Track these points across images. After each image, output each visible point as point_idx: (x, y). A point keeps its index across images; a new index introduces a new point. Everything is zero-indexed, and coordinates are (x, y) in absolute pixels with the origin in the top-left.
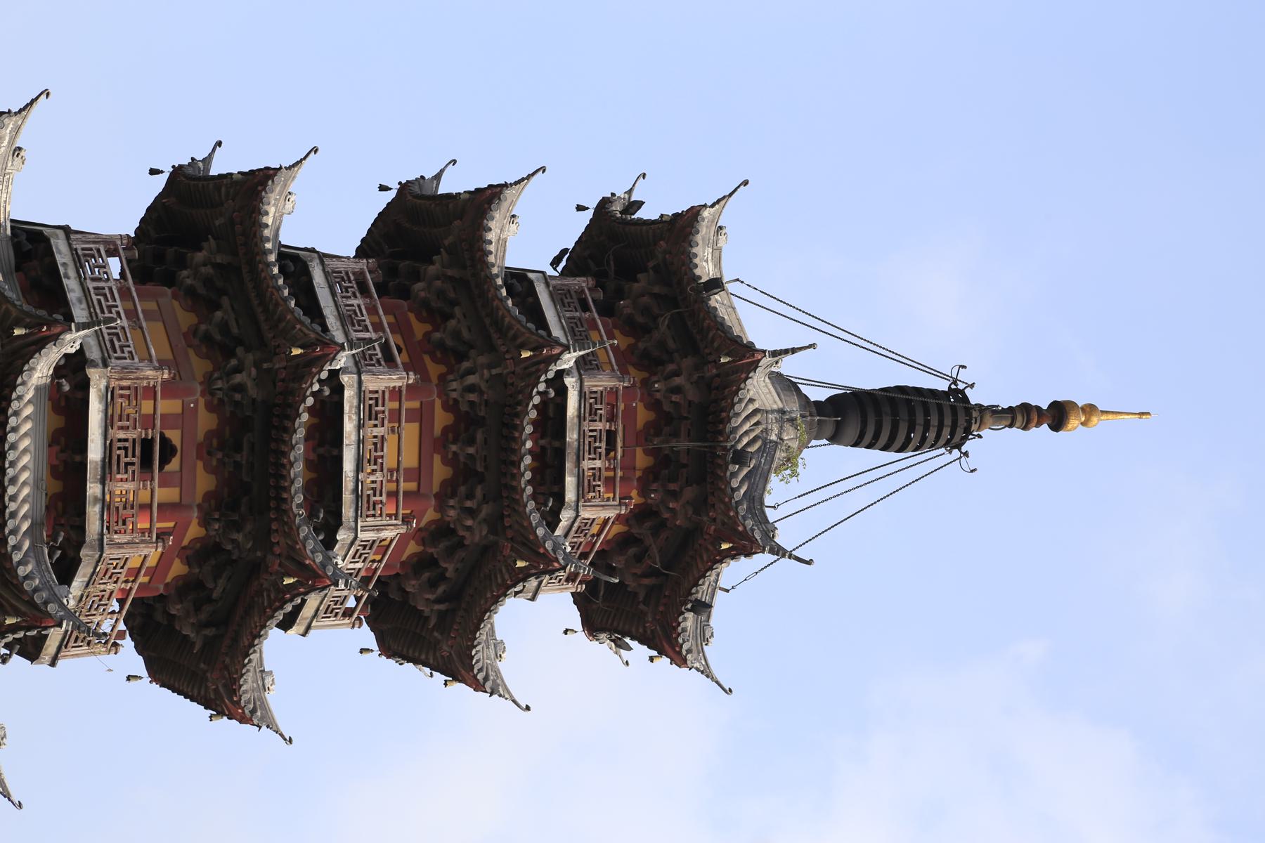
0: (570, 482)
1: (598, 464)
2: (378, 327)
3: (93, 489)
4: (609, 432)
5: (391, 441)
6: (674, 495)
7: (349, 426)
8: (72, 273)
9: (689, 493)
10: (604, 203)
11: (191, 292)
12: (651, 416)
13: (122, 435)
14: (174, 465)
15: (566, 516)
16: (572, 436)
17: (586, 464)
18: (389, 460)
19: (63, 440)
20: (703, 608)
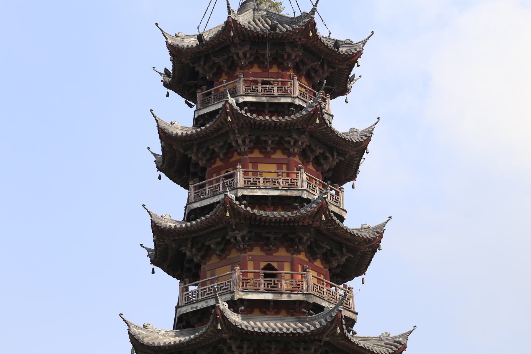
0: (283, 100)
1: (276, 88)
2: (218, 181)
3: (285, 297)
4: (263, 84)
6: (289, 56)
7: (259, 193)
9: (288, 49)
10: (166, 85)
11: (203, 257)
12: (256, 66)
13: (262, 286)
14: (275, 265)
15: (298, 102)
16: (264, 99)
17: (276, 93)
18: (274, 176)
19: (264, 310)
20: (337, 44)
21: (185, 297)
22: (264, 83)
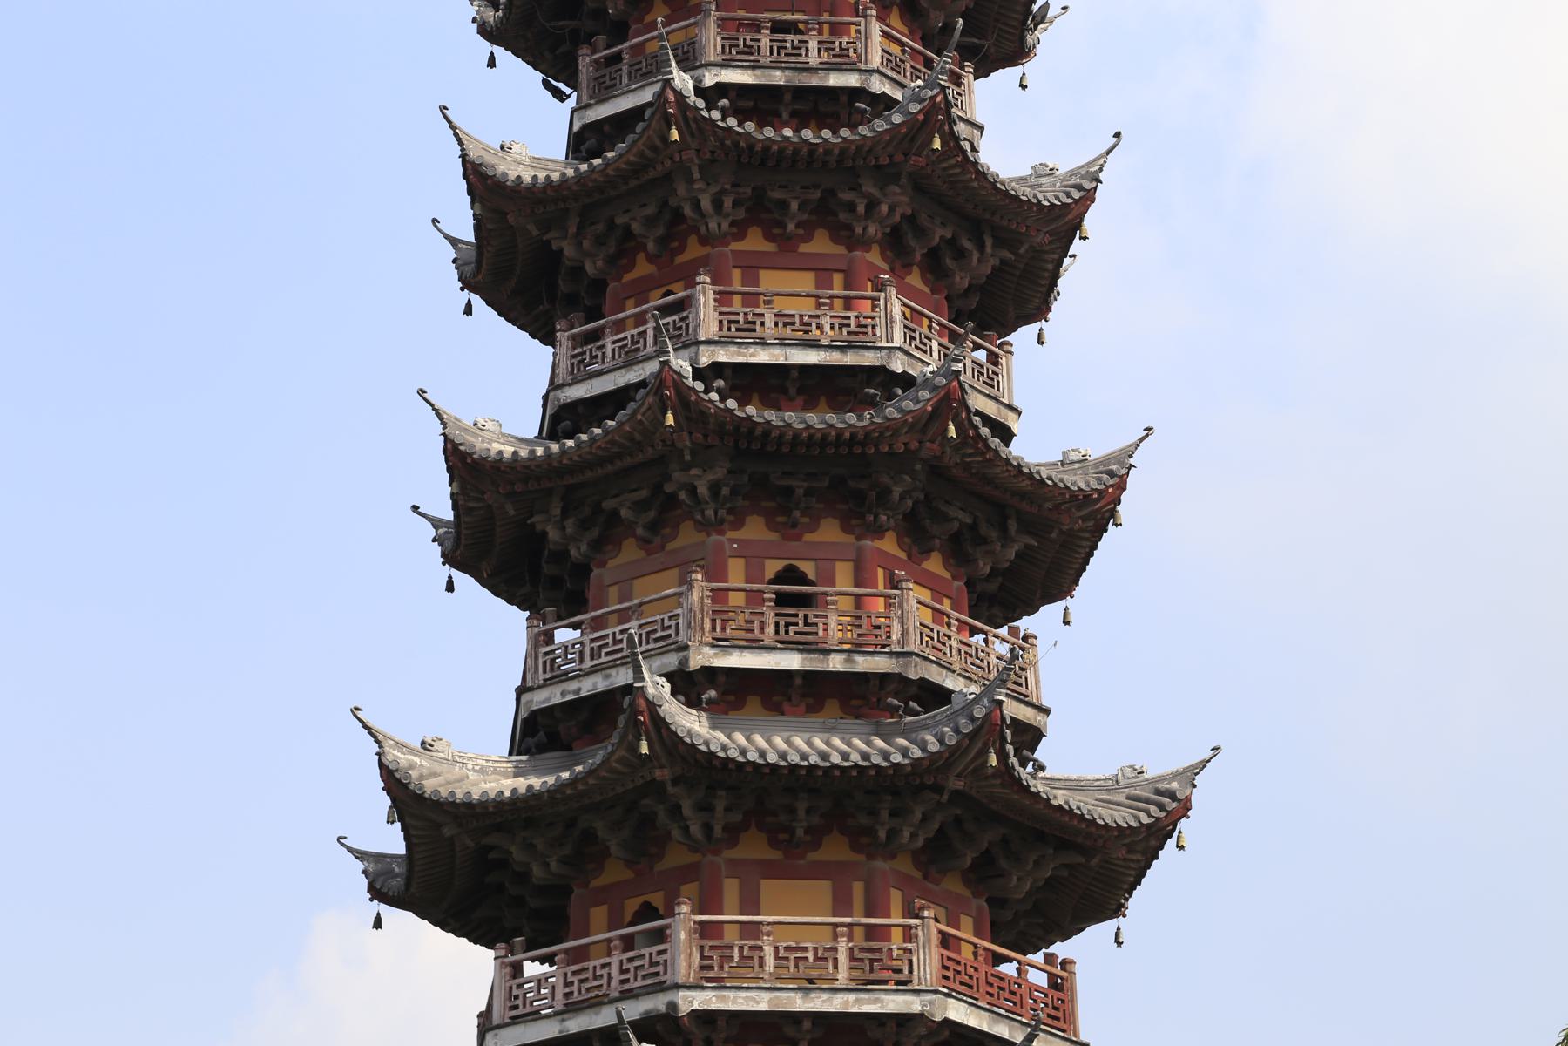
0: (835, 80)
1: (813, 44)
2: (640, 319)
3: (836, 663)
5: (782, 305)
7: (763, 356)
8: (573, 685)
11: (597, 545)
13: (770, 630)
14: (808, 568)
15: (878, 86)
16: (778, 78)
17: (813, 60)
18: (805, 307)
21: (543, 663)
22: (779, 28)
